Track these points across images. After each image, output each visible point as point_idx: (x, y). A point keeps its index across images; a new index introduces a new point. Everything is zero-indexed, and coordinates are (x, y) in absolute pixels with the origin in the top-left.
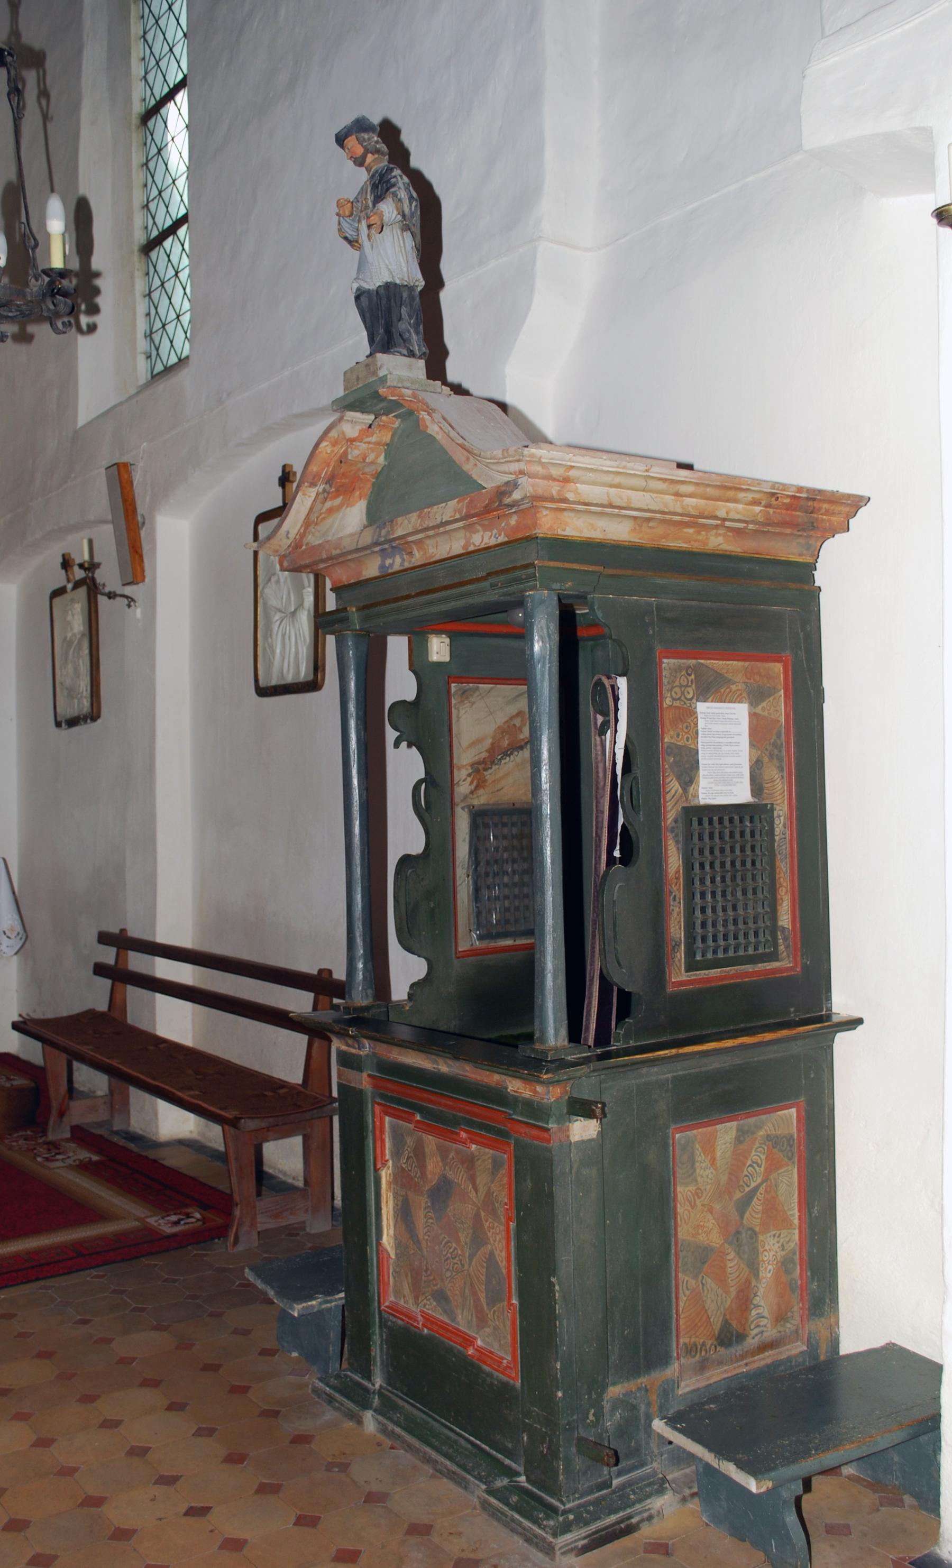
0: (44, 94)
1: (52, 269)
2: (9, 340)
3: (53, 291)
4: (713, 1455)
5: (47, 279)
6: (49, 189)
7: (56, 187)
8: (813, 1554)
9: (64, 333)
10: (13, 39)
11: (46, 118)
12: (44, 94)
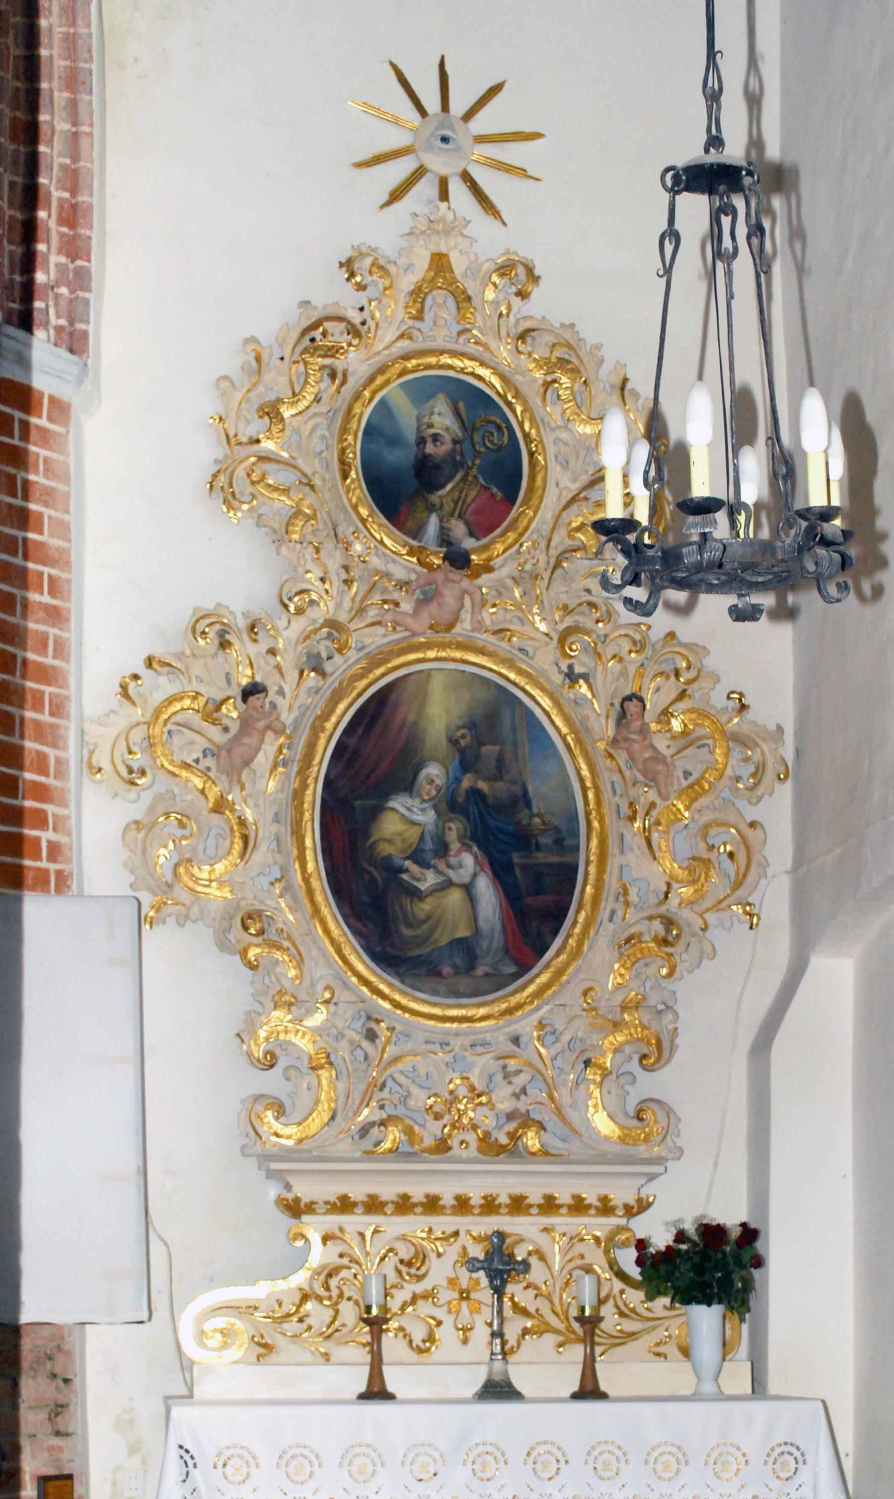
0: (797, 233)
1: (809, 509)
2: (764, 617)
3: (815, 538)
4: (37, 911)
5: (804, 524)
6: (805, 378)
7: (817, 380)
8: (812, 1396)
9: (838, 600)
10: (753, 153)
11: (801, 270)
12: (797, 233)
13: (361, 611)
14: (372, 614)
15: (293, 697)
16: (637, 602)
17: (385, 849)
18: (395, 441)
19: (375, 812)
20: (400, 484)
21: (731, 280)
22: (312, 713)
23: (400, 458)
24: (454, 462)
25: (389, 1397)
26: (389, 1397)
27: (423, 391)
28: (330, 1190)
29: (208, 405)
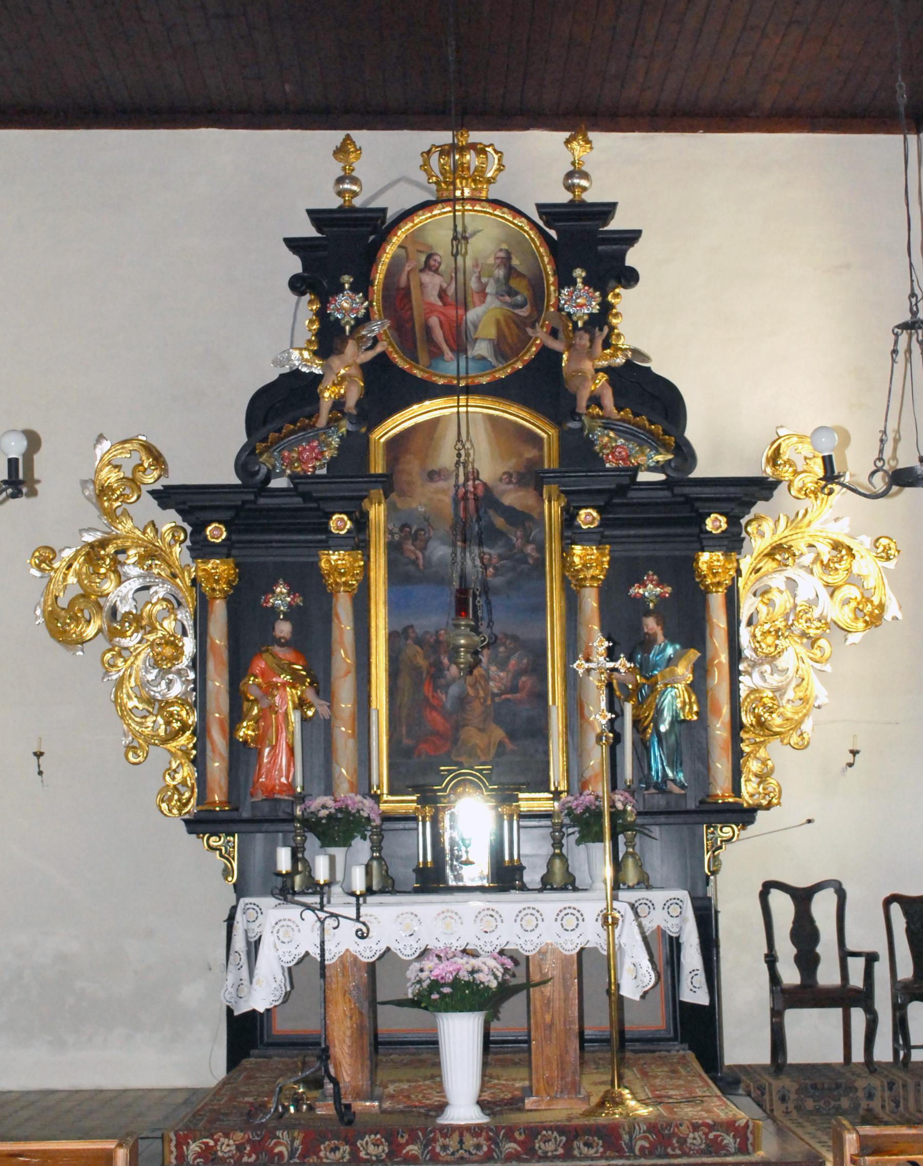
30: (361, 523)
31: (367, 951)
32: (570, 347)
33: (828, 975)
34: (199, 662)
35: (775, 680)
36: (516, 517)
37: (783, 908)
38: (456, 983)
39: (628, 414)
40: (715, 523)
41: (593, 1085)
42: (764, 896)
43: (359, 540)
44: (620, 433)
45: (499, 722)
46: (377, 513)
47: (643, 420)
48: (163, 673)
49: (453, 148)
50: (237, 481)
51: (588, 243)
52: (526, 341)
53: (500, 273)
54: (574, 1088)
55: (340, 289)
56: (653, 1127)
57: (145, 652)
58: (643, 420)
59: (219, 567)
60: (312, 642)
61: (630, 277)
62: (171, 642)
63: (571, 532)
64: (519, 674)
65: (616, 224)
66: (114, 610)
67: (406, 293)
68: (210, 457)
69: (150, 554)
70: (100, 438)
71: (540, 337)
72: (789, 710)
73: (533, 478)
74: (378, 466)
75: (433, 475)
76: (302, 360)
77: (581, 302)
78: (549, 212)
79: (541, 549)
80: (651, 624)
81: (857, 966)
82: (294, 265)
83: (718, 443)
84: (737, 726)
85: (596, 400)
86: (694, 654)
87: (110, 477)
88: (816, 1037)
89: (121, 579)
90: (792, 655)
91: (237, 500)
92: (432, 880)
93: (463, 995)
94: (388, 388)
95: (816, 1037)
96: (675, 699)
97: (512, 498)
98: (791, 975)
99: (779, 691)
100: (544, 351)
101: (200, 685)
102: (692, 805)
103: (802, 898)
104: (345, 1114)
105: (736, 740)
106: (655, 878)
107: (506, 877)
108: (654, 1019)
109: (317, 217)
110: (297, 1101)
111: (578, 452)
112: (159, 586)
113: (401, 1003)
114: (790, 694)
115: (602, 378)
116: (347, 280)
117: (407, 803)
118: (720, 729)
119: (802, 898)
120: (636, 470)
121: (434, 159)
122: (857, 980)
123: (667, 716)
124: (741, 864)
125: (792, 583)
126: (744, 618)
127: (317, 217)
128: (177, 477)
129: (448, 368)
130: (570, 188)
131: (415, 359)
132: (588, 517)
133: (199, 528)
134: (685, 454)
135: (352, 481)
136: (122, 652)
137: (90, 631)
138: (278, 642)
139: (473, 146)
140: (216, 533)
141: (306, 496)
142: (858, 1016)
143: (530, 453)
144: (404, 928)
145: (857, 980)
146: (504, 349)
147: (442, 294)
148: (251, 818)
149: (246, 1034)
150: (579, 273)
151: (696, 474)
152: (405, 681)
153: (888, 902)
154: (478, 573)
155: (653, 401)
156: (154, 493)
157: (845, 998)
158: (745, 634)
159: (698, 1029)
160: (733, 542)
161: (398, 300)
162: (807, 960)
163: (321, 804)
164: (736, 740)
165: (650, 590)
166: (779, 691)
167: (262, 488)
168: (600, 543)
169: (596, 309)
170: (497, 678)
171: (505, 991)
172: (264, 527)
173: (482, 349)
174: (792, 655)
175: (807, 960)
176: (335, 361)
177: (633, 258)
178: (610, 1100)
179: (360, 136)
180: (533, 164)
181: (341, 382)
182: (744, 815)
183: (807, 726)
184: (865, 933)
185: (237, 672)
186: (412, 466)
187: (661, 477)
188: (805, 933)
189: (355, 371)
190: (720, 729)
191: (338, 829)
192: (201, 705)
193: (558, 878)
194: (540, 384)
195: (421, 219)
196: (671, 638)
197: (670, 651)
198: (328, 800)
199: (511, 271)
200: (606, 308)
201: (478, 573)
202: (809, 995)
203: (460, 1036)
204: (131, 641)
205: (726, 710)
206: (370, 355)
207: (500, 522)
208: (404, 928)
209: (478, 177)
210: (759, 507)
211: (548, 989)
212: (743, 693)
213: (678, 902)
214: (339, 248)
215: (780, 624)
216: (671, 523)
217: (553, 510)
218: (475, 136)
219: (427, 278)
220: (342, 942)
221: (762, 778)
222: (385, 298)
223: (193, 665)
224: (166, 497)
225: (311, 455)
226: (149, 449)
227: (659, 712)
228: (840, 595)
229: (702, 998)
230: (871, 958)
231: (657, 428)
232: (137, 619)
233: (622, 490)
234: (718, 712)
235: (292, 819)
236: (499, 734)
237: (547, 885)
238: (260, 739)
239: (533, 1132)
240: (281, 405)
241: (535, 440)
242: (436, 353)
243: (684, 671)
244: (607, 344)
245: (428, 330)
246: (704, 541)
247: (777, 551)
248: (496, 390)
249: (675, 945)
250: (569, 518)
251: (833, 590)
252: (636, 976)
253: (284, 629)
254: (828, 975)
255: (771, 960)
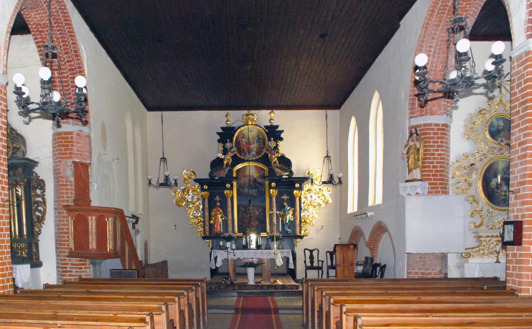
13: (488, 152)
14: (490, 152)
15: (478, 165)
16: (45, 195)
17: (492, 186)
18: (494, 127)
19: (490, 181)
20: (494, 134)
21: (134, 150)
22: (481, 167)
23: (494, 129)
24: (503, 130)
25: (499, 262)
26: (499, 262)
27: (498, 119)
28: (486, 235)
29: (463, 124)
30: (232, 185)
31: (235, 258)
32: (270, 153)
33: (315, 264)
34: (203, 210)
35: (308, 213)
36: (260, 184)
37: (308, 253)
38: (250, 263)
39: (281, 165)
40: (297, 185)
41: (272, 280)
42: (304, 251)
43: (231, 188)
44: (279, 169)
45: (258, 221)
46: (235, 183)
47: (284, 167)
48: (197, 212)
49: (247, 115)
50: (209, 178)
51: (274, 133)
52: (262, 152)
53: (257, 138)
54: (269, 280)
55: (227, 142)
56: (282, 285)
57: (193, 208)
58: (284, 167)
59: (206, 193)
60: (224, 206)
61: (281, 139)
62: (198, 206)
63: (270, 187)
64: (261, 212)
65: (279, 129)
66: (188, 201)
67: (239, 142)
68: (204, 173)
69: (194, 191)
70: (184, 170)
71: (265, 151)
72: (310, 219)
73: (263, 177)
74: (235, 175)
75: (245, 176)
76: (220, 155)
77: (272, 144)
78: (266, 127)
79: (265, 190)
80: (285, 204)
81: (320, 263)
82: (218, 137)
83: (298, 168)
84: (301, 222)
85: (275, 163)
86: (293, 209)
87: (186, 177)
88: (313, 274)
89: (189, 195)
90: (311, 209)
91: (208, 181)
92: (246, 247)
93: (251, 265)
94: (236, 160)
95: (313, 274)
96: (289, 217)
97: (259, 180)
98: (308, 264)
99: (308, 216)
100: (265, 153)
101: (204, 214)
102: (292, 235)
103: (311, 251)
104: (232, 283)
105: (300, 224)
106: (285, 248)
107: (258, 247)
108: (284, 271)
109: (223, 128)
110: (224, 281)
111: (272, 172)
112: (195, 197)
113: (241, 266)
114: (311, 216)
115: (276, 159)
116: (228, 140)
117: (241, 234)
118: (298, 222)
119: (311, 251)
120: (283, 175)
121: (244, 117)
122: (320, 265)
123: (288, 220)
124: (300, 246)
125: (311, 196)
126: (302, 202)
127: (223, 128)
128: (198, 177)
129: (247, 157)
130: (270, 122)
131: (241, 155)
132: (273, 184)
133: (202, 186)
134: (291, 172)
135: (229, 178)
136: (190, 208)
137: (184, 204)
138: (217, 206)
139: (251, 114)
140: (206, 187)
141: (222, 181)
142: (320, 271)
143: (263, 172)
144: (241, 254)
145: (320, 265)
146: (258, 153)
147: (246, 142)
148: (214, 237)
149: (214, 272)
150: (272, 139)
151: (293, 176)
152: (240, 213)
153: (327, 252)
154: (253, 193)
155: (286, 162)
156: (194, 180)
157: (319, 268)
158: (302, 205)
159: (292, 273)
160: (300, 189)
161: (238, 143)
162: (312, 262)
163: (226, 235)
164: (300, 224)
165: (285, 197)
166: (308, 216)
167: (214, 179)
168: (275, 189)
169: (275, 145)
170: (257, 213)
171: (258, 265)
172: (214, 186)
173: (254, 153)
174: (311, 209)
175: (312, 262)
176: (226, 156)
177: (282, 135)
178: (275, 281)
179: (230, 112)
180: (264, 117)
181: (228, 159)
182: (301, 237)
183: (314, 222)
184: (322, 257)
185: (210, 212)
186: (241, 174)
187: (287, 177)
188: (311, 257)
189: (230, 158)
190: (298, 222)
191: (229, 239)
192: (204, 217)
193: (268, 248)
194: (265, 160)
195: (242, 128)
196: (289, 206)
197: (288, 208)
198: (227, 234)
199: (259, 138)
200: (277, 145)
201: (253, 193)
202: (312, 268)
203: (251, 271)
204: (191, 206)
205: (298, 219)
206: (233, 155)
207: (257, 185)
208: (241, 254)
209: (252, 120)
210: (305, 182)
211: (265, 264)
212: (302, 216)
213: (289, 252)
214: (226, 134)
215: (309, 203)
216: (289, 185)
217: (267, 183)
218: (252, 112)
219: (243, 140)
220: (231, 256)
221: (305, 231)
222: (235, 144)
223: (202, 210)
224: (196, 180)
225: (223, 173)
226: (193, 172)
227: (286, 219)
228: (320, 198)
229: (293, 267)
230: (323, 262)
231: (287, 168)
232: (192, 202)
233: (280, 179)
234: (297, 219)
235: (221, 237)
236: (257, 223)
237: (266, 249)
238: (215, 223)
239: (263, 286)
240: (217, 164)
241: (264, 170)
242: (245, 154)
243: (291, 212)
244: (277, 152)
245: (244, 149)
246: (295, 188)
247: (309, 190)
248: (256, 161)
249: (288, 259)
250: (270, 184)
251: (319, 197)
252: (280, 262)
253: (218, 204)
254: (315, 264)
255: (305, 262)
